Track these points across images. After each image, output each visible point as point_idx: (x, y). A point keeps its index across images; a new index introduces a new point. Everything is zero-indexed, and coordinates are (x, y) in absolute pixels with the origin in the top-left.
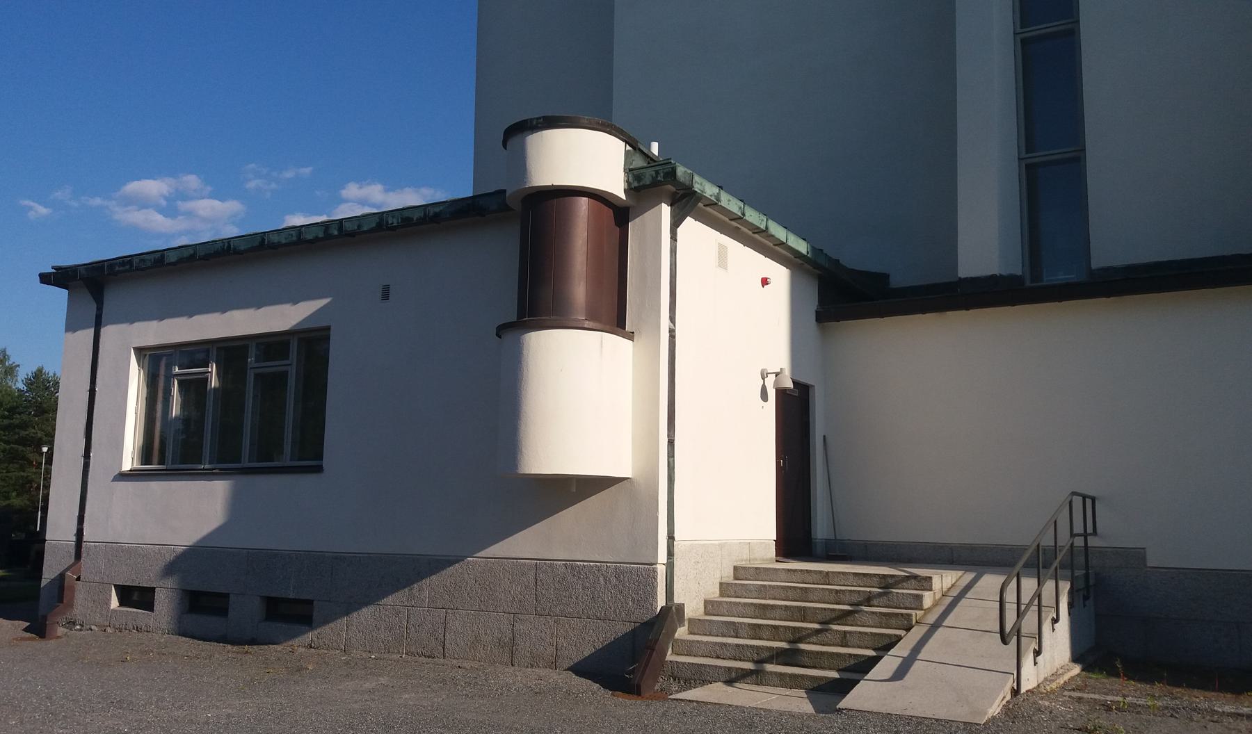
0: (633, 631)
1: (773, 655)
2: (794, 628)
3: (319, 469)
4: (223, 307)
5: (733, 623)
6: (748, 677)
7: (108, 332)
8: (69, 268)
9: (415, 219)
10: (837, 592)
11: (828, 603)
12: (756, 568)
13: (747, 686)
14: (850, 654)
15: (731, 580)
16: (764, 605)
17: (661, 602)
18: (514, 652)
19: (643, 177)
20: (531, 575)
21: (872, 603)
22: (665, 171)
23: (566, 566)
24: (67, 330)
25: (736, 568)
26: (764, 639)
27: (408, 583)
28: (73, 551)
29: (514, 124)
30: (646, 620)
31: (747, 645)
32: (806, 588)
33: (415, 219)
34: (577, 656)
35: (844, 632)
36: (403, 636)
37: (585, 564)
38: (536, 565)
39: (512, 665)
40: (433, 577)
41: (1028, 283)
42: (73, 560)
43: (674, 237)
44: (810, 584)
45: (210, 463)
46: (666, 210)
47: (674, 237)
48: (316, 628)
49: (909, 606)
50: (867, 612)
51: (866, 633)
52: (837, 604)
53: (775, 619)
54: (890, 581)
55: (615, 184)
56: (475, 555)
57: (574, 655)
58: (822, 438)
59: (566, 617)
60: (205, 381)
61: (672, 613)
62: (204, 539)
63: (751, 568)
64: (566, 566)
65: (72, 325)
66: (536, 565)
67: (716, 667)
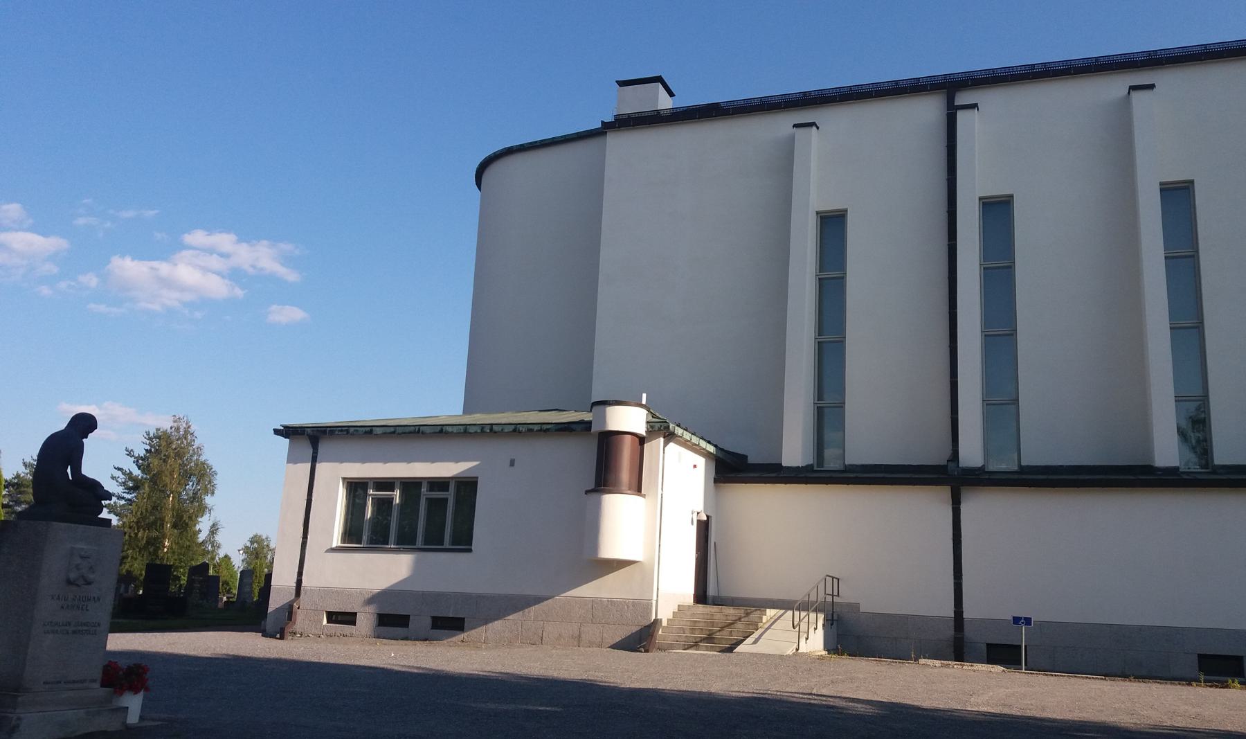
3: (470, 550)
4: (409, 460)
7: (321, 467)
8: (292, 428)
15: (677, 611)
17: (653, 618)
20: (590, 606)
24: (288, 462)
25: (679, 606)
27: (522, 608)
28: (294, 592)
40: (537, 606)
41: (815, 468)
42: (293, 597)
43: (664, 450)
45: (367, 544)
46: (662, 440)
47: (664, 450)
48: (467, 631)
55: (641, 429)
58: (589, 495)
60: (390, 500)
61: (657, 622)
62: (392, 586)
65: (292, 459)
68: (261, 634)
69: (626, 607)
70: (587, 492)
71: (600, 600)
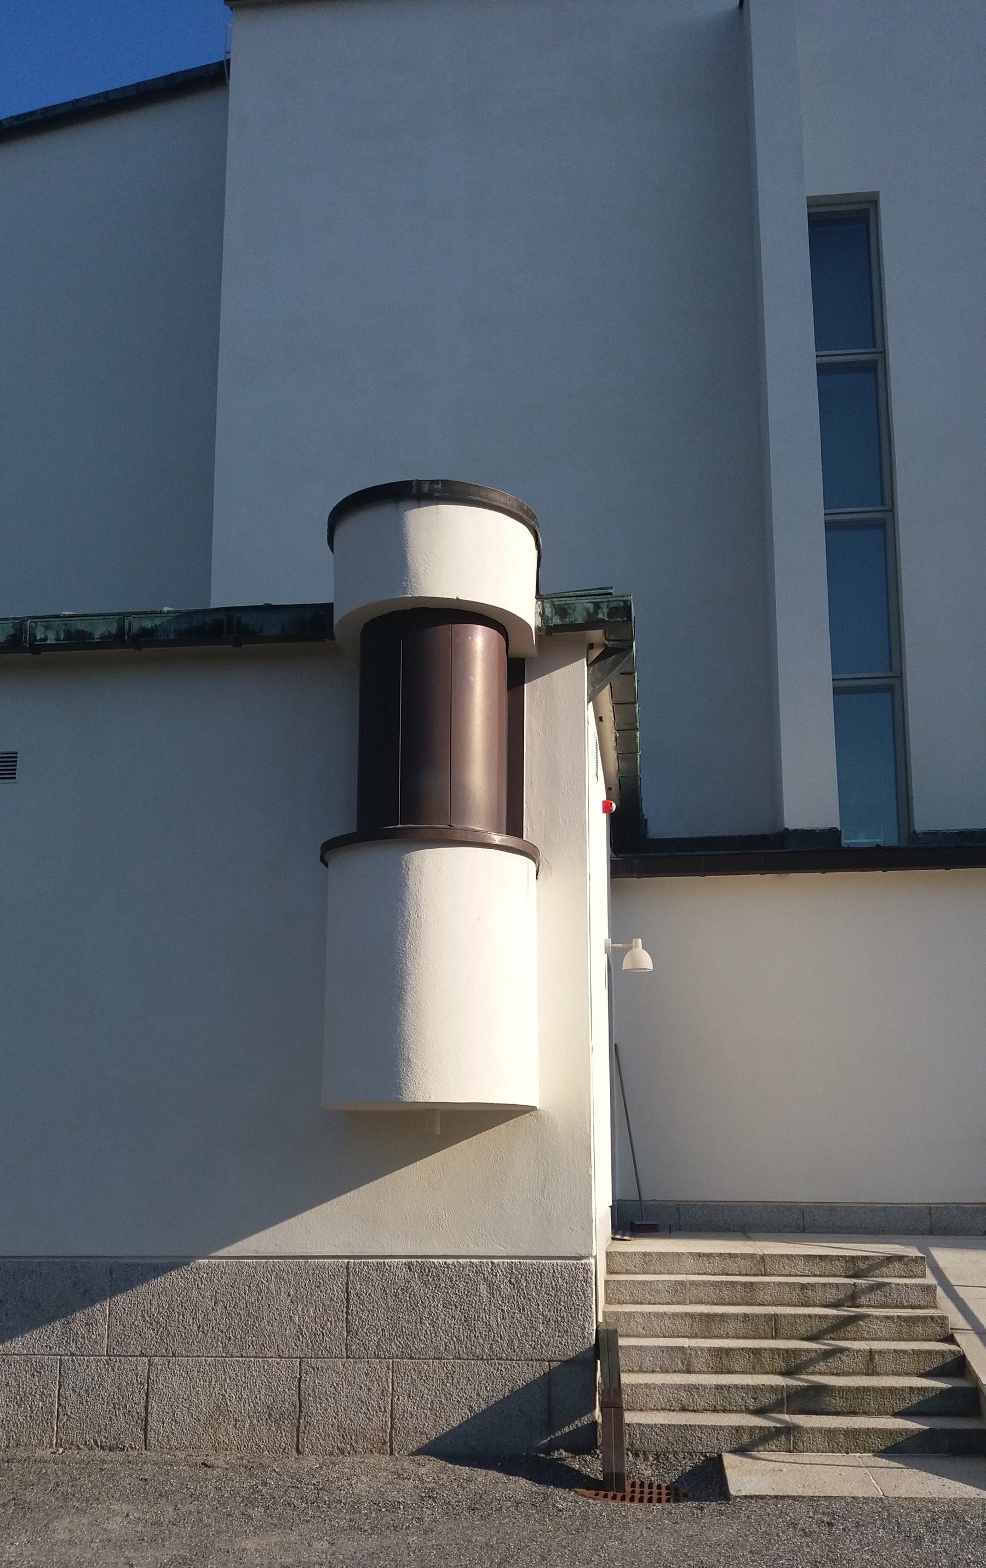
0: (549, 1376)
1: (782, 1399)
2: (787, 1350)
4: (468, 686)
5: (682, 1349)
6: (772, 1440)
9: (97, 636)
10: (803, 1287)
11: (789, 1305)
12: (645, 1254)
13: (773, 1456)
14: (911, 1388)
16: (707, 1315)
18: (302, 1428)
19: (571, 611)
20: (337, 1286)
21: (858, 1301)
22: (611, 605)
23: (410, 1267)
26: (736, 1372)
29: (350, 496)
30: (572, 1355)
31: (736, 1387)
32: (752, 1283)
33: (97, 636)
34: (433, 1430)
35: (871, 1351)
36: (51, 1413)
37: (449, 1261)
38: (347, 1268)
39: (298, 1451)
40: (120, 1298)
44: (736, 1275)
49: (917, 1303)
50: (877, 1317)
51: (905, 1352)
52: (803, 1305)
53: (727, 1337)
54: (862, 1265)
56: (213, 1255)
57: (429, 1425)
59: (412, 1358)
63: (635, 1254)
64: (410, 1267)
66: (347, 1268)
67: (714, 1428)
68: (845, 842)
69: (483, 1288)
70: (331, 847)
71: (381, 1263)
